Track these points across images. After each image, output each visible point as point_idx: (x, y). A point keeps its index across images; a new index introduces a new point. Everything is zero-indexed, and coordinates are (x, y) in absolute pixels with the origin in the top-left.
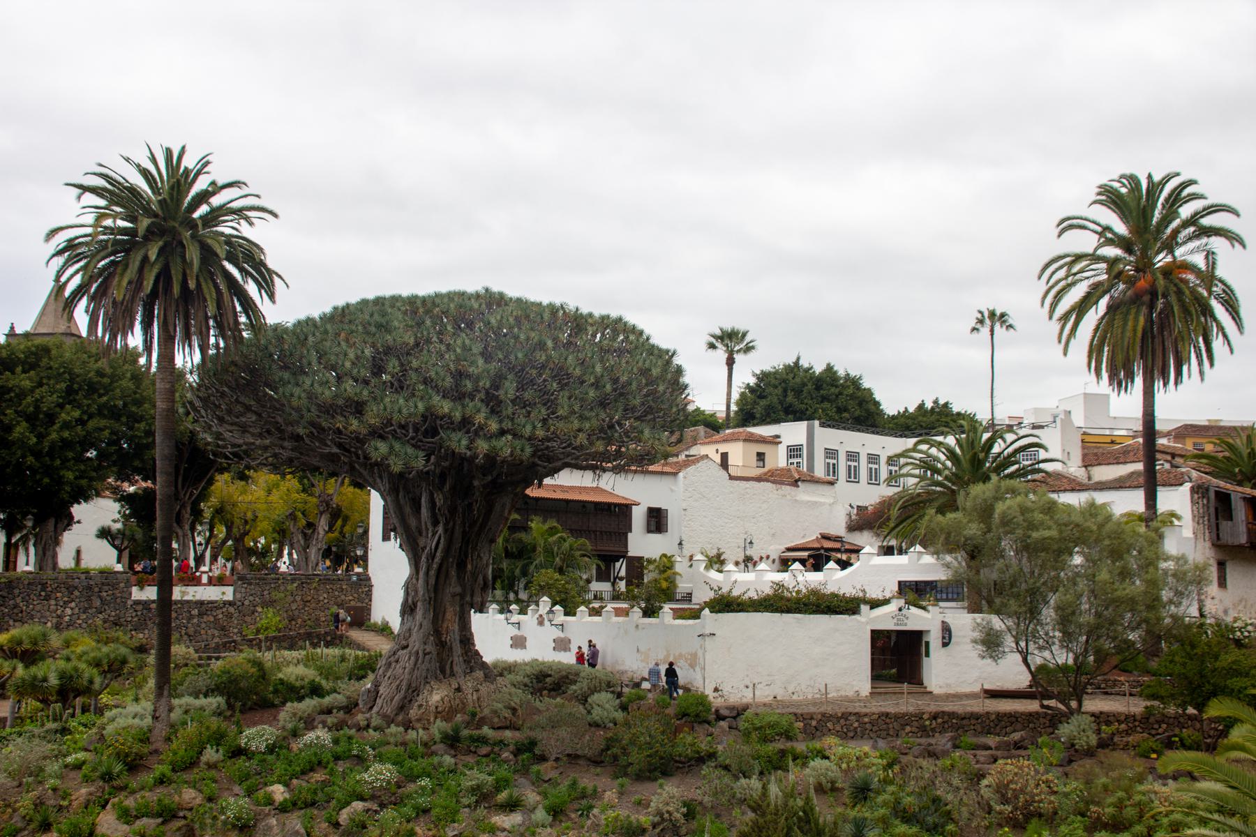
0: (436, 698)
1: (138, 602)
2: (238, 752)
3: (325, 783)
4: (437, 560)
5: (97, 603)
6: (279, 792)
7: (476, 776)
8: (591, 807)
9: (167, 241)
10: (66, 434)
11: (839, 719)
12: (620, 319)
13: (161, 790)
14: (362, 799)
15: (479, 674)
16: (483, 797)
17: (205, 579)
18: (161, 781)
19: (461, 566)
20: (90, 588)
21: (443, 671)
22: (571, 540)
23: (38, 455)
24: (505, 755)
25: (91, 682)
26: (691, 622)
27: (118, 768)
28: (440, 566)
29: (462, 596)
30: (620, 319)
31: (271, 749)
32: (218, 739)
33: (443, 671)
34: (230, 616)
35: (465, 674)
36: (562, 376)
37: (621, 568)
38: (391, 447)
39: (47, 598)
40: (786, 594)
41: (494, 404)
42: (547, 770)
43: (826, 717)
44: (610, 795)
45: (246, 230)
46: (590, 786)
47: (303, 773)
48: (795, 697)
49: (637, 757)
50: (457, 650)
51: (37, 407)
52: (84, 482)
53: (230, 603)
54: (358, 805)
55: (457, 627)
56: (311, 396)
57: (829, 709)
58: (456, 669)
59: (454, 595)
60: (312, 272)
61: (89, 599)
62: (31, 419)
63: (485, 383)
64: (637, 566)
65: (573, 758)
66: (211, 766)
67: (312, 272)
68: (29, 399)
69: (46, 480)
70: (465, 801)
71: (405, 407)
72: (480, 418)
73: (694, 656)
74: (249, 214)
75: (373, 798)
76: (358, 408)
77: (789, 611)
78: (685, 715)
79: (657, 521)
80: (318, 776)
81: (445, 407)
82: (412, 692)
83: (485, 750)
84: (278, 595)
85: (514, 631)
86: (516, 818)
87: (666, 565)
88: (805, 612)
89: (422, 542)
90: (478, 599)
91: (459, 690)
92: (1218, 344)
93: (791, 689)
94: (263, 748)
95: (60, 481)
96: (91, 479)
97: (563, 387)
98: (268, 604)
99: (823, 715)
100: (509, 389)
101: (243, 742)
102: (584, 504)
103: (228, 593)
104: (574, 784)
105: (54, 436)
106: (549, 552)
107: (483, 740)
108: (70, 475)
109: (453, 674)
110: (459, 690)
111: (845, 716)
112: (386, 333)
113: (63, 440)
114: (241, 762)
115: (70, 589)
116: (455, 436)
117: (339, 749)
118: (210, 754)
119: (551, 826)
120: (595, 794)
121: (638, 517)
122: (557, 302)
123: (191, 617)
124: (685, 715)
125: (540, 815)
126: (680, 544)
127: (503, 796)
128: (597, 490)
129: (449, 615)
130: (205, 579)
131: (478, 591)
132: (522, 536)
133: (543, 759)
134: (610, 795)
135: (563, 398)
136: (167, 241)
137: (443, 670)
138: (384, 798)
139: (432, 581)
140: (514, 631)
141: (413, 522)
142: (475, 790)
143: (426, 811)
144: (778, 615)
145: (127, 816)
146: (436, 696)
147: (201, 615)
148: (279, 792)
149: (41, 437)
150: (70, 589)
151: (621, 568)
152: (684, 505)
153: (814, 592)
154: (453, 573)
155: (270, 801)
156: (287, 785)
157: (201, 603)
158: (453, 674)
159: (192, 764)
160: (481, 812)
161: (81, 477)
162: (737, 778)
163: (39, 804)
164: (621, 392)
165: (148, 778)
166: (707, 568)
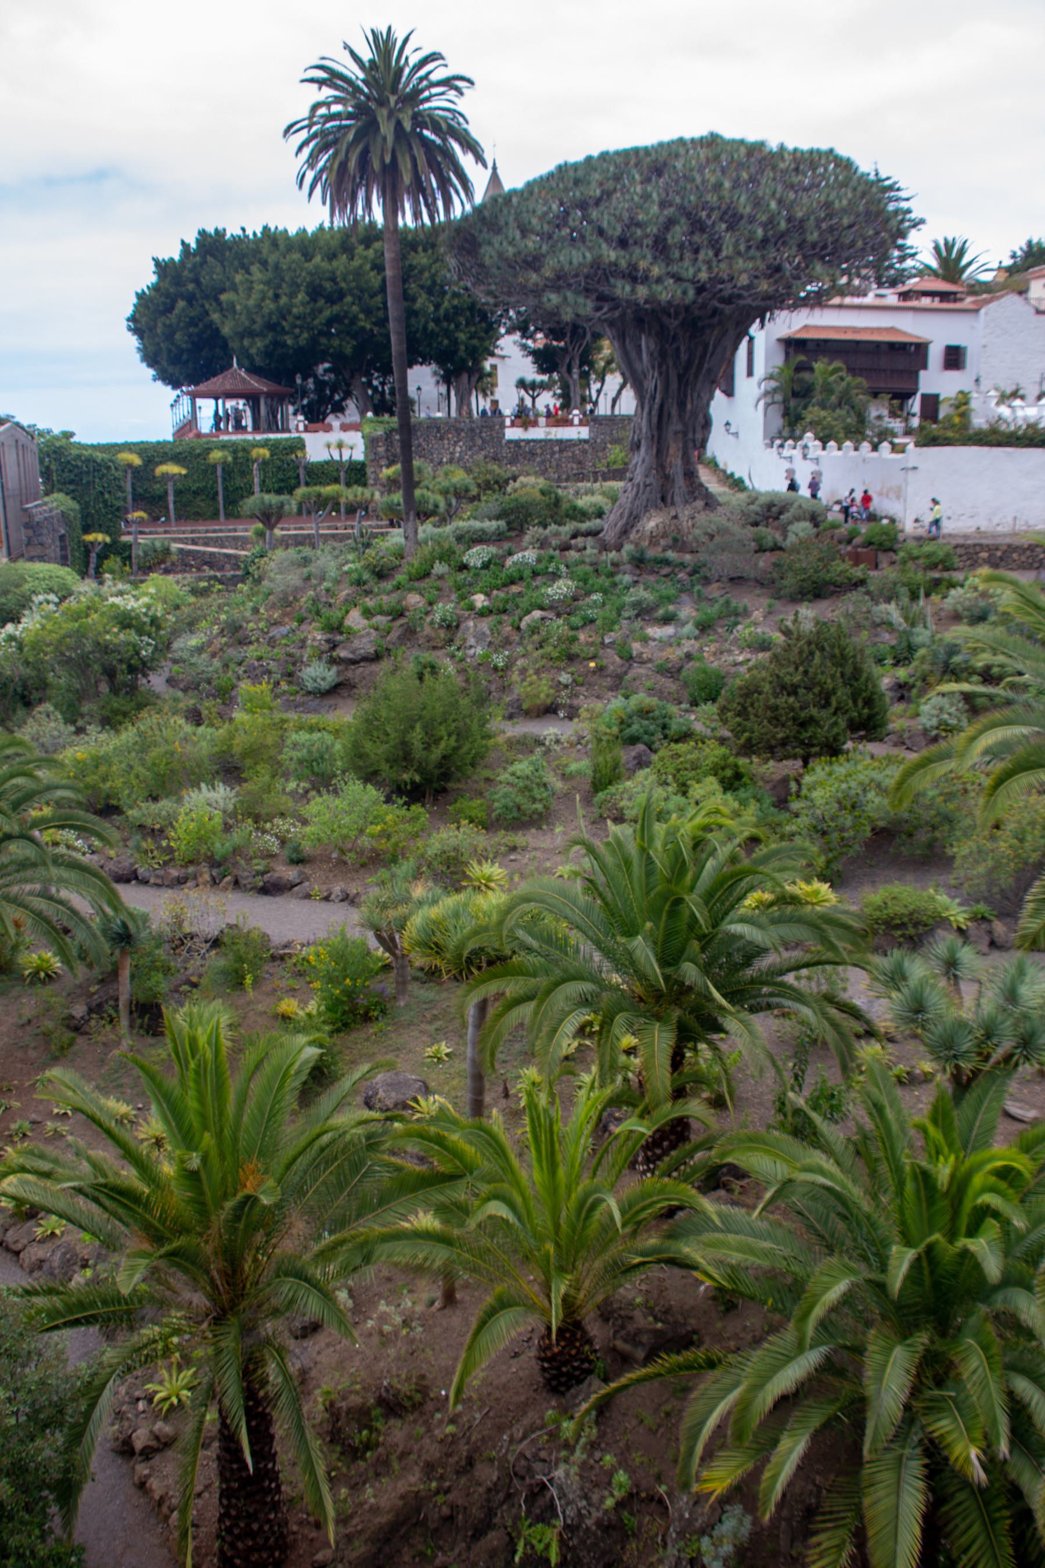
0: (652, 524)
1: (510, 442)
2: (463, 567)
3: (520, 594)
4: (658, 400)
5: (479, 442)
6: (480, 600)
7: (641, 593)
8: (736, 624)
9: (383, 121)
10: (456, 302)
11: (1025, 550)
12: (831, 151)
13: (395, 595)
14: (542, 609)
15: (700, 504)
16: (644, 612)
17: (576, 421)
18: (398, 587)
19: (682, 405)
20: (472, 430)
21: (663, 499)
22: (849, 379)
23: (437, 321)
24: (681, 575)
25: (436, 506)
26: (900, 456)
27: (366, 576)
28: (662, 406)
29: (685, 433)
30: (831, 151)
31: (486, 566)
32: (446, 556)
33: (663, 499)
34: (585, 452)
35: (686, 502)
36: (733, 219)
37: (915, 405)
38: (565, 298)
39: (442, 439)
40: (1003, 427)
41: (660, 247)
42: (714, 591)
43: (1011, 549)
44: (757, 615)
45: (462, 105)
46: (741, 606)
47: (505, 585)
48: (999, 529)
49: (790, 582)
50: (680, 482)
51: (434, 282)
52: (475, 342)
53: (585, 441)
54: (537, 614)
55: (679, 462)
56: (501, 255)
57: (1016, 541)
58: (677, 499)
59: (676, 433)
60: (523, 127)
61: (472, 439)
62: (430, 291)
63: (652, 230)
64: (931, 403)
65: (737, 580)
66: (440, 577)
67: (523, 127)
68: (426, 275)
69: (446, 342)
70: (626, 614)
71: (576, 257)
72: (643, 265)
73: (899, 488)
74: (460, 84)
75: (551, 608)
76: (533, 262)
77: (999, 445)
78: (870, 543)
79: (954, 358)
80: (515, 589)
81: (611, 254)
82: (633, 519)
83: (666, 570)
84: (622, 434)
85: (786, 465)
86: (669, 630)
87: (963, 402)
88: (1017, 446)
89: (646, 384)
90: (699, 436)
91: (675, 517)
92: (366, 54)
93: (995, 521)
94: (479, 564)
95: (456, 342)
96: (481, 339)
97: (731, 228)
98: (616, 441)
99: (1009, 546)
100: (677, 234)
101: (465, 559)
102: (878, 344)
103: (584, 433)
104: (728, 602)
105: (446, 304)
106: (828, 389)
107: (667, 562)
108: (462, 336)
109: (673, 503)
110: (675, 517)
111: (1032, 548)
112: (581, 189)
113: (455, 307)
114: (461, 576)
115: (458, 431)
116: (619, 283)
117: (540, 566)
118: (439, 568)
119: (696, 638)
120: (746, 613)
121: (935, 355)
122: (752, 137)
123: (553, 454)
124: (870, 543)
125: (689, 628)
126: (977, 380)
127: (661, 612)
128: (892, 330)
129: (671, 451)
130: (576, 421)
131: (699, 429)
132: (806, 376)
133: (706, 581)
134: (757, 615)
135: (728, 239)
136: (383, 121)
137: (664, 499)
138: (562, 608)
139: (655, 420)
140: (786, 465)
141: (638, 366)
142: (636, 604)
143: (592, 621)
144: (986, 449)
145: (368, 613)
146: (652, 523)
147: (561, 451)
148: (480, 600)
149: (437, 306)
150: (458, 431)
151: (915, 405)
152: (984, 342)
153: (1032, 426)
154: (674, 412)
155: (471, 607)
156: (488, 595)
157: (560, 442)
158: (673, 503)
159: (427, 575)
160: (638, 624)
161: (471, 338)
162: (877, 604)
163: (315, 601)
164: (798, 226)
165: (388, 585)
166: (998, 404)
